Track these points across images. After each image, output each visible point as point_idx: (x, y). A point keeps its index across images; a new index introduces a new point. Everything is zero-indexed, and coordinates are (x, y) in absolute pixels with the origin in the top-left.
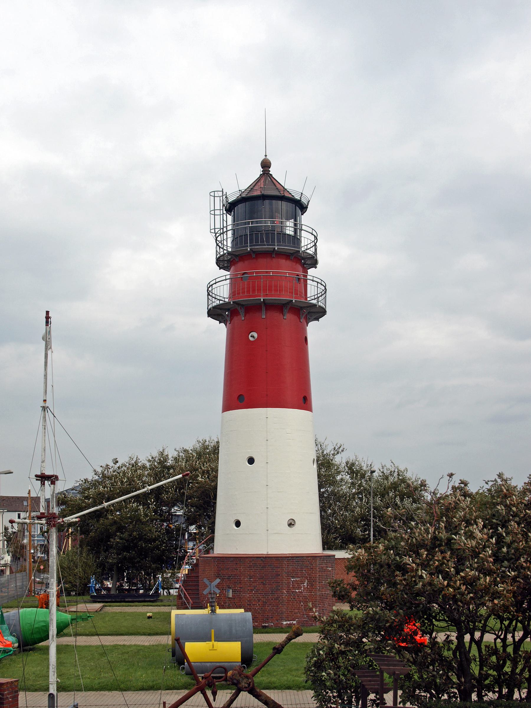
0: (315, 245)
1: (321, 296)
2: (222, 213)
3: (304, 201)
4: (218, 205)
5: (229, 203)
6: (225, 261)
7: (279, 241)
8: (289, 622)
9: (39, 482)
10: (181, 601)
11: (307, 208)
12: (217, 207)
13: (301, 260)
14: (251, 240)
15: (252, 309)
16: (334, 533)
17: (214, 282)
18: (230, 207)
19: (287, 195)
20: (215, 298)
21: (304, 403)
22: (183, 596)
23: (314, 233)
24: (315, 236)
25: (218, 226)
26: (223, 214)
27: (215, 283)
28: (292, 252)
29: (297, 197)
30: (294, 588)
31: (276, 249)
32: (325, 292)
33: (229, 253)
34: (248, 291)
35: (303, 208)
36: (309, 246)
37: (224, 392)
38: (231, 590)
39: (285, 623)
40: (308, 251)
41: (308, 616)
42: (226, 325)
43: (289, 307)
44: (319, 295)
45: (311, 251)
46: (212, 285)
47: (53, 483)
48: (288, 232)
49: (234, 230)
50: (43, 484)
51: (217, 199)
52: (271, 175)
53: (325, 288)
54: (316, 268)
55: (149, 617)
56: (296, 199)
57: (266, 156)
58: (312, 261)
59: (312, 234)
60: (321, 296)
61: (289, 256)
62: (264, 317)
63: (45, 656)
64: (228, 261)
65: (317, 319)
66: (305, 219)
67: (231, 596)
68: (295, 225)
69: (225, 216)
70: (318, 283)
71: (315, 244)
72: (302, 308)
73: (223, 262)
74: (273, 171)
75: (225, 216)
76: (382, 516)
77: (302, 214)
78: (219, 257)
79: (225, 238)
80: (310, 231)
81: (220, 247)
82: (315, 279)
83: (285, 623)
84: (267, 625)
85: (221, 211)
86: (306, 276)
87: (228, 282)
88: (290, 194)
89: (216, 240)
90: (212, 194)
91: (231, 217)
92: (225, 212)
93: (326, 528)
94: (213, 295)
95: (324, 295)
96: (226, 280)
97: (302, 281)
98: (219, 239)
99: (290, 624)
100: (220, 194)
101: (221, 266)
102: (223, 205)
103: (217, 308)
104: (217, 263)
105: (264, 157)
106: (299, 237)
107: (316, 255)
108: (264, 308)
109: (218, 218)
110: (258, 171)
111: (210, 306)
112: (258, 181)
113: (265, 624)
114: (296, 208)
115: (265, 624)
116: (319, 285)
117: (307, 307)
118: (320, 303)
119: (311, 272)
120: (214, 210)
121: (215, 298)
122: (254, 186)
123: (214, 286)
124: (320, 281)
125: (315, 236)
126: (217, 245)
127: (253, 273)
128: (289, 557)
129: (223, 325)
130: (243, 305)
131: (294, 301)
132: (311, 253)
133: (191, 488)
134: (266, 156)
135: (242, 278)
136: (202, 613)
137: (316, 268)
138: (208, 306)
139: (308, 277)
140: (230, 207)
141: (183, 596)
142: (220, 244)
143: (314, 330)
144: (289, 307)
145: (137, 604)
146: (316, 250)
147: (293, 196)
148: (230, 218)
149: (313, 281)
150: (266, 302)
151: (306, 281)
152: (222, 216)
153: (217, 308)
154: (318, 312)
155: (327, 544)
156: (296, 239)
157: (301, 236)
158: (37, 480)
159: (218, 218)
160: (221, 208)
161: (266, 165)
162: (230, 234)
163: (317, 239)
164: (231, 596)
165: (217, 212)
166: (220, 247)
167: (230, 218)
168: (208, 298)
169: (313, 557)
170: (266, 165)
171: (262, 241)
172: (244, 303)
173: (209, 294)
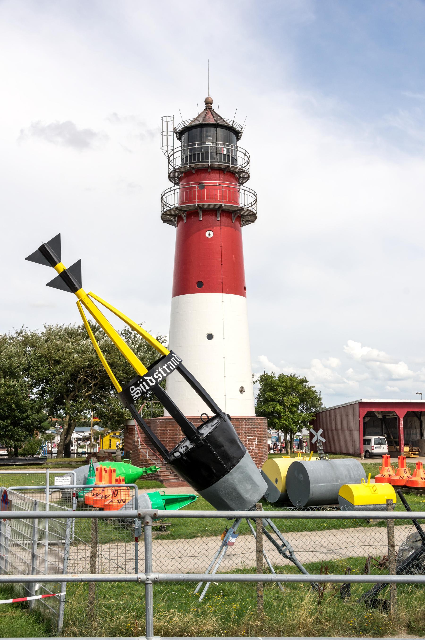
14: (190, 160)
15: (192, 213)
17: (169, 190)
20: (166, 205)
21: (237, 287)
27: (164, 195)
28: (225, 167)
29: (231, 124)
31: (210, 164)
35: (238, 134)
37: (174, 273)
43: (220, 210)
61: (234, 174)
62: (201, 219)
63: (216, 434)
70: (245, 190)
74: (214, 107)
76: (74, 376)
87: (178, 191)
89: (169, 160)
105: (207, 96)
108: (201, 213)
110: (204, 106)
116: (246, 192)
121: (166, 205)
130: (184, 211)
131: (223, 206)
136: (235, 434)
140: (180, 134)
143: (247, 232)
144: (220, 210)
145: (243, 417)
149: (249, 192)
150: (202, 207)
154: (251, 217)
161: (208, 103)
170: (208, 103)
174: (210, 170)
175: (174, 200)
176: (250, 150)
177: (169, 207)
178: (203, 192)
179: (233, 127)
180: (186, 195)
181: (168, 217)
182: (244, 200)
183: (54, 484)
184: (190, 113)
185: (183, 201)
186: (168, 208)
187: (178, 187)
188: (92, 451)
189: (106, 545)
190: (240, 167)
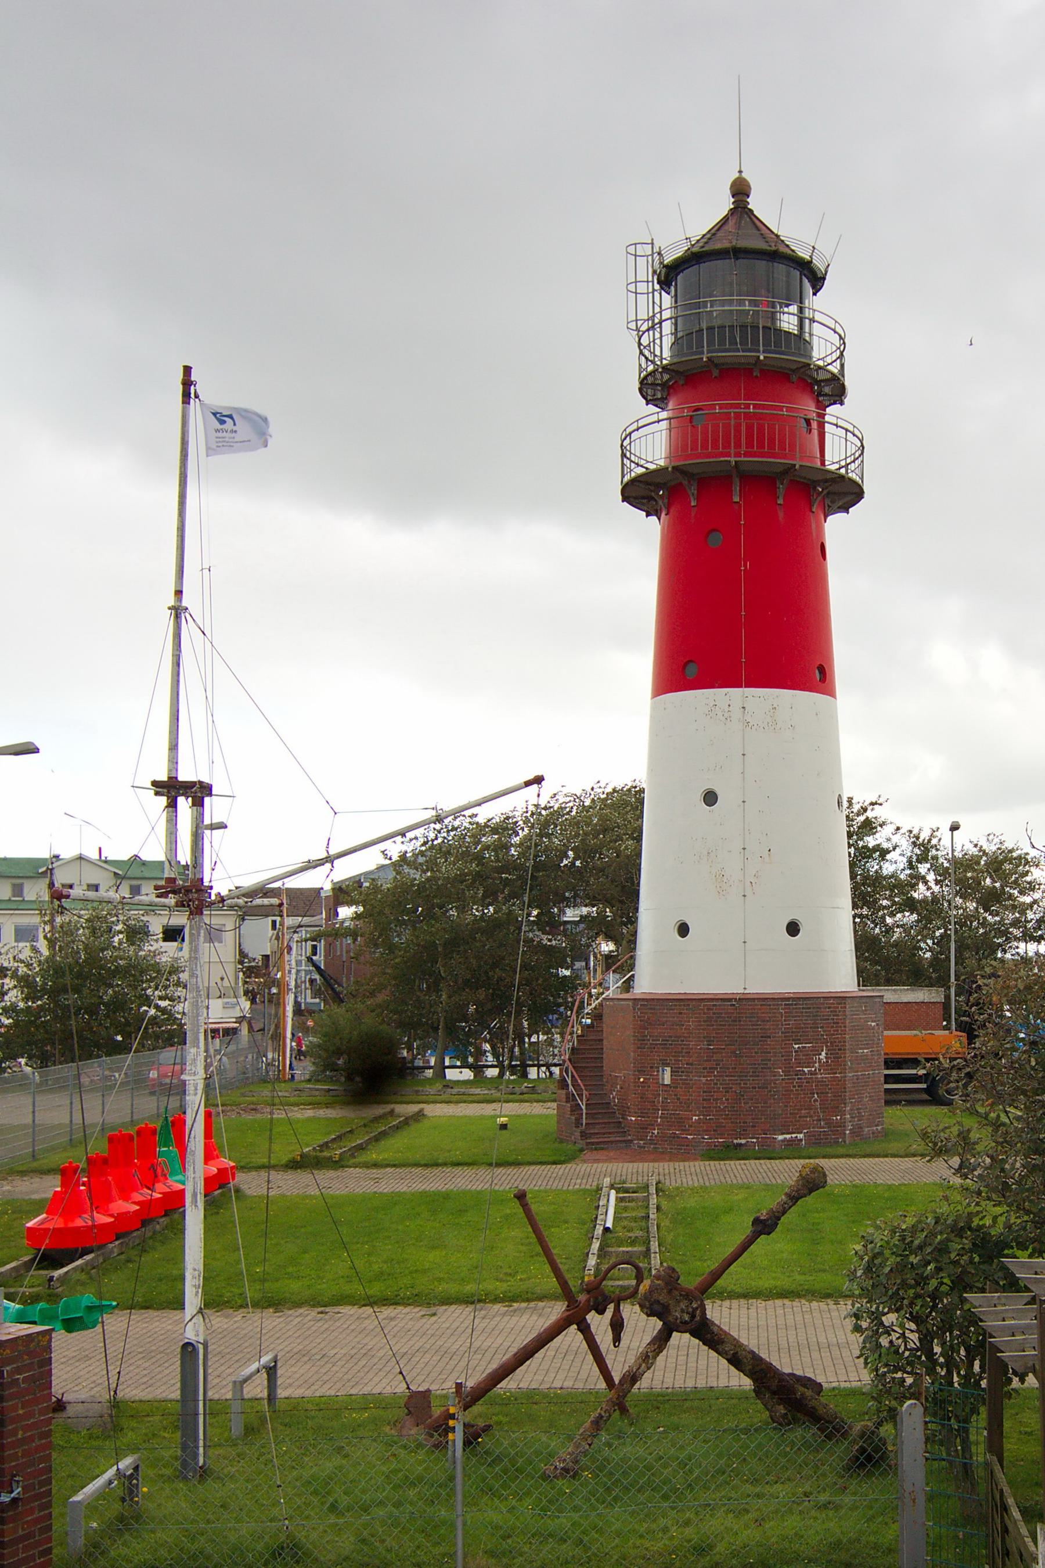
0: (841, 356)
1: (854, 462)
2: (650, 290)
3: (819, 263)
4: (644, 271)
5: (665, 266)
6: (658, 385)
7: (767, 344)
8: (788, 1136)
9: (163, 801)
10: (564, 1092)
11: (824, 279)
12: (642, 275)
13: (811, 386)
16: (876, 958)
17: (634, 426)
18: (667, 275)
19: (782, 249)
22: (569, 1082)
23: (839, 329)
24: (840, 336)
25: (643, 315)
26: (654, 290)
27: (637, 430)
28: (794, 367)
29: (804, 254)
30: (799, 1064)
31: (762, 358)
32: (862, 453)
33: (665, 368)
34: (705, 446)
35: (817, 281)
36: (829, 360)
38: (669, 1069)
39: (780, 1137)
40: (830, 368)
41: (829, 1123)
42: (659, 519)
44: (849, 460)
45: (834, 369)
46: (630, 434)
47: (198, 803)
48: (785, 326)
49: (675, 319)
50: (172, 805)
51: (642, 261)
52: (751, 211)
53: (862, 445)
54: (842, 403)
55: (504, 1127)
56: (802, 259)
57: (740, 172)
58: (835, 390)
59: (835, 332)
60: (854, 462)
64: (664, 385)
65: (845, 509)
66: (819, 303)
67: (667, 1081)
68: (801, 310)
69: (657, 294)
70: (847, 430)
71: (842, 353)
72: (815, 483)
73: (656, 387)
75: (657, 294)
77: (815, 294)
78: (645, 378)
79: (657, 335)
80: (832, 324)
81: (647, 358)
82: (840, 423)
83: (780, 1137)
84: (743, 1141)
85: (650, 284)
86: (823, 416)
87: (664, 425)
88: (788, 246)
90: (632, 250)
91: (669, 297)
92: (657, 287)
93: (860, 972)
94: (633, 458)
95: (860, 459)
96: (658, 422)
97: (814, 425)
98: (645, 341)
99: (791, 1140)
100: (648, 249)
101: (649, 398)
102: (654, 272)
103: (641, 482)
104: (641, 390)
105: (737, 175)
106: (807, 339)
107: (843, 376)
109: (642, 299)
110: (725, 204)
111: (627, 478)
112: (725, 221)
113: (739, 1141)
114: (801, 279)
115: (739, 1141)
117: (826, 481)
118: (850, 475)
119: (833, 411)
120: (636, 282)
122: (718, 230)
123: (634, 436)
124: (851, 428)
125: (840, 336)
126: (641, 353)
127: (713, 407)
128: (788, 999)
129: (654, 518)
131: (797, 467)
132: (835, 371)
133: (588, 860)
134: (740, 172)
135: (691, 417)
137: (842, 403)
138: (623, 476)
139: (827, 418)
140: (669, 275)
141: (569, 1082)
142: (646, 353)
143: (837, 530)
146: (842, 366)
147: (793, 251)
148: (667, 300)
149: (837, 426)
151: (821, 426)
152: (651, 295)
153: (641, 482)
154: (845, 493)
155: (864, 977)
156: (800, 341)
157: (811, 335)
158: (157, 794)
159: (642, 299)
160: (650, 279)
161: (740, 190)
162: (667, 327)
163: (844, 343)
164: (667, 1081)
165: (642, 288)
166: (647, 358)
167: (667, 300)
168: (623, 464)
169: (841, 999)
170: (740, 190)
171: (733, 342)
172: (695, 471)
173: (623, 455)
174: (716, 373)
175: (655, 450)
176: (837, 323)
177: (642, 466)
178: (761, 428)
179: (811, 262)
180: (686, 436)
181: (641, 492)
182: (835, 454)
183: (14, 885)
184: (695, 215)
185: (684, 448)
186: (640, 471)
187: (664, 415)
188: (666, 1166)
189: (552, 1275)
190: (821, 363)
